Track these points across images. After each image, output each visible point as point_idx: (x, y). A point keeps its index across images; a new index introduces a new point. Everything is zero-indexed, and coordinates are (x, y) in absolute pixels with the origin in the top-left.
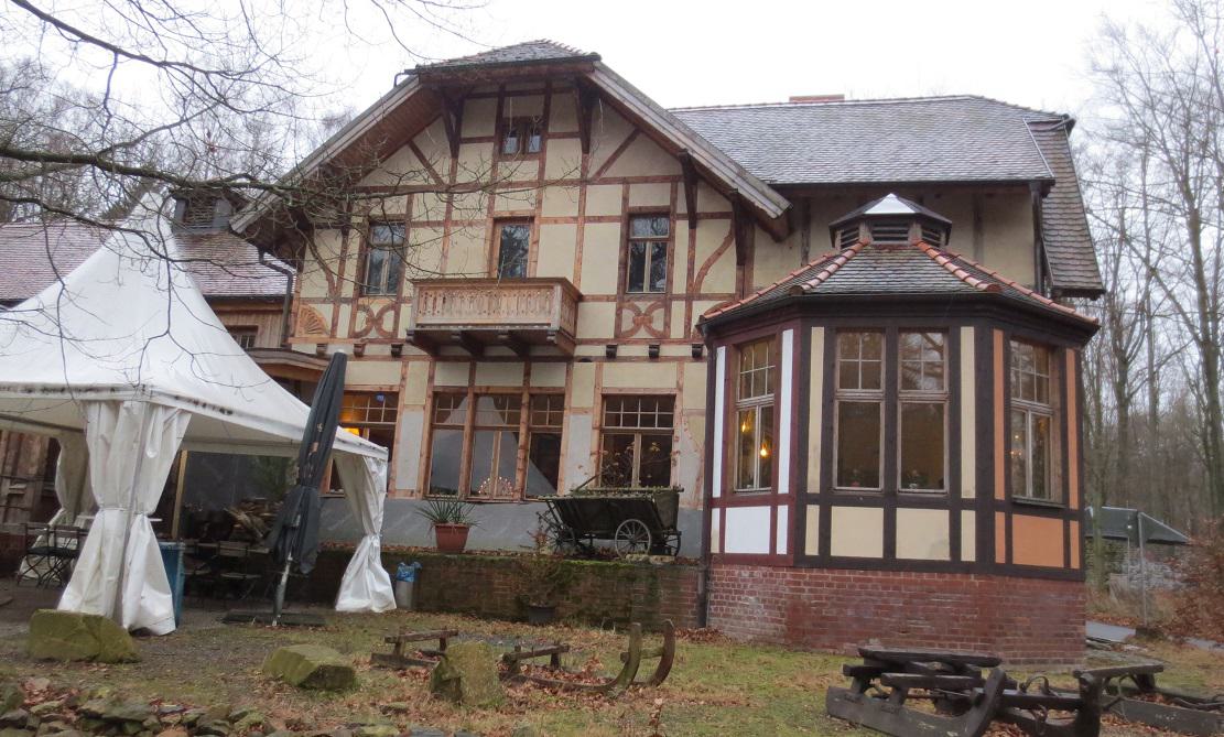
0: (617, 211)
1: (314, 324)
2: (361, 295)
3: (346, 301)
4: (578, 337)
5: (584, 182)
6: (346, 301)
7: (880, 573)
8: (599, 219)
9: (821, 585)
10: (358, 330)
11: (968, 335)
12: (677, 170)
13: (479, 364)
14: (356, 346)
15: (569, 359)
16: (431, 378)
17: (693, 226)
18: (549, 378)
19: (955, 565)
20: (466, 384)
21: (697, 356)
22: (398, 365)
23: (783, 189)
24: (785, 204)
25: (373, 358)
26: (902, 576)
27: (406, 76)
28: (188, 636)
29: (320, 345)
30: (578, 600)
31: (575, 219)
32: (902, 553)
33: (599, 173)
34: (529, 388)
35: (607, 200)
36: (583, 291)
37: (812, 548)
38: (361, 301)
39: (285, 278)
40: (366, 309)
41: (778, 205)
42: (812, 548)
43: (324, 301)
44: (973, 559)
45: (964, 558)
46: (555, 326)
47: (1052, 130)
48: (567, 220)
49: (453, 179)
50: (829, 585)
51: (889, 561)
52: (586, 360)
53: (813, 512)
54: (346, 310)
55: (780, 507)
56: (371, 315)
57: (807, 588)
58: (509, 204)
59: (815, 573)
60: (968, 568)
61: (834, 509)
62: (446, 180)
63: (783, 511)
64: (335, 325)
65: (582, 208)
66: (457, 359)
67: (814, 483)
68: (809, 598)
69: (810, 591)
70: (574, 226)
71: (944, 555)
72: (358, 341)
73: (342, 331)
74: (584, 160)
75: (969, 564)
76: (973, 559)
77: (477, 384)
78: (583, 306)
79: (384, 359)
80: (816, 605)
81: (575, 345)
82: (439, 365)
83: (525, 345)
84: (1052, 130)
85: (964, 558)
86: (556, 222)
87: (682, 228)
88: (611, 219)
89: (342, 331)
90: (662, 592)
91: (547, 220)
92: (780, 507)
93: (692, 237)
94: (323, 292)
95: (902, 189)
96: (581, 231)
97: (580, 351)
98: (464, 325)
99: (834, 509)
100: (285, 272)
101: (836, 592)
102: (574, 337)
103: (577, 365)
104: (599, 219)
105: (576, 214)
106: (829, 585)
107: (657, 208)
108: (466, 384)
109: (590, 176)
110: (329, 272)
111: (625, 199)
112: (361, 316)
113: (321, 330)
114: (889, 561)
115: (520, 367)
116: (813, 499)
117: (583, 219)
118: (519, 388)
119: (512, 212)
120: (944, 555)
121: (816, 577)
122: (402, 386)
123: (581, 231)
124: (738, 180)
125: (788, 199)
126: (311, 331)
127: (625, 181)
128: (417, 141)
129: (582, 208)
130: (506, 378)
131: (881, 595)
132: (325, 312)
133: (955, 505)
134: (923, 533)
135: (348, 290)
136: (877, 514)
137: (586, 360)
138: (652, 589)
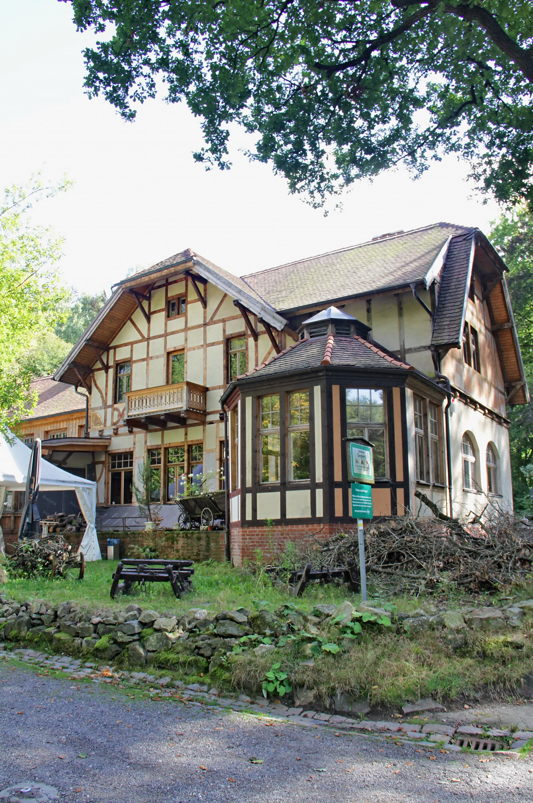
0: (221, 338)
1: (97, 422)
2: (115, 402)
3: (109, 406)
4: (208, 411)
5: (205, 325)
6: (109, 406)
7: (279, 527)
8: (213, 344)
9: (254, 535)
10: (115, 421)
11: (317, 390)
12: (238, 312)
13: (165, 432)
14: (114, 429)
15: (204, 423)
16: (146, 442)
17: (256, 340)
18: (195, 434)
19: (313, 520)
20: (160, 443)
21: (222, 419)
22: (132, 436)
23: (282, 313)
24: (285, 321)
25: (122, 435)
26: (289, 527)
27: (117, 287)
28: (240, 597)
29: (100, 431)
30: (178, 551)
31: (202, 346)
32: (289, 516)
33: (212, 319)
34: (187, 442)
35: (216, 333)
36: (208, 386)
37: (249, 517)
38: (116, 406)
39: (85, 398)
40: (117, 410)
41: (281, 322)
42: (249, 517)
43: (101, 408)
44: (322, 516)
45: (317, 516)
46: (185, 408)
47: (464, 240)
48: (199, 348)
49: (149, 334)
50: (258, 535)
51: (283, 521)
52: (211, 423)
53: (249, 496)
54: (109, 410)
55: (317, 490)
56: (119, 412)
57: (248, 537)
58: (175, 342)
59: (251, 529)
60: (319, 521)
61: (258, 494)
62: (146, 337)
63: (319, 493)
64: (105, 420)
65: (205, 339)
66: (156, 430)
67: (249, 484)
68: (249, 542)
69: (250, 539)
70: (202, 350)
71: (308, 515)
72: (115, 427)
73: (109, 423)
74: (205, 313)
75: (320, 518)
76: (322, 516)
77: (165, 442)
78: (209, 393)
79: (126, 435)
80: (252, 546)
81: (206, 415)
82: (149, 434)
83: (176, 419)
84: (464, 240)
85: (317, 516)
86: (194, 349)
87: (251, 340)
88: (218, 343)
89: (109, 423)
90: (212, 545)
91: (190, 349)
92: (317, 490)
93: (256, 346)
94: (100, 403)
95: (340, 303)
96: (205, 352)
97: (209, 418)
98: (166, 410)
99: (258, 494)
100: (84, 395)
101: (261, 538)
102: (205, 411)
103: (208, 426)
104: (213, 344)
105: (202, 344)
106: (258, 535)
107: (239, 333)
108: (160, 443)
109: (207, 321)
110: (102, 394)
111: (224, 331)
112: (116, 413)
113: (100, 424)
114: (283, 521)
115: (182, 431)
116: (338, 485)
117: (207, 345)
118: (183, 442)
119: (175, 348)
120: (308, 515)
121: (252, 531)
122: (134, 448)
123: (205, 352)
124: (262, 312)
125: (285, 318)
126: (96, 424)
127: (224, 321)
128: (133, 317)
129: (205, 339)
130: (175, 437)
131: (280, 538)
132: (101, 414)
133: (313, 487)
134: (299, 504)
135: (110, 402)
136: (308, 492)
137: (211, 423)
138: (208, 544)
